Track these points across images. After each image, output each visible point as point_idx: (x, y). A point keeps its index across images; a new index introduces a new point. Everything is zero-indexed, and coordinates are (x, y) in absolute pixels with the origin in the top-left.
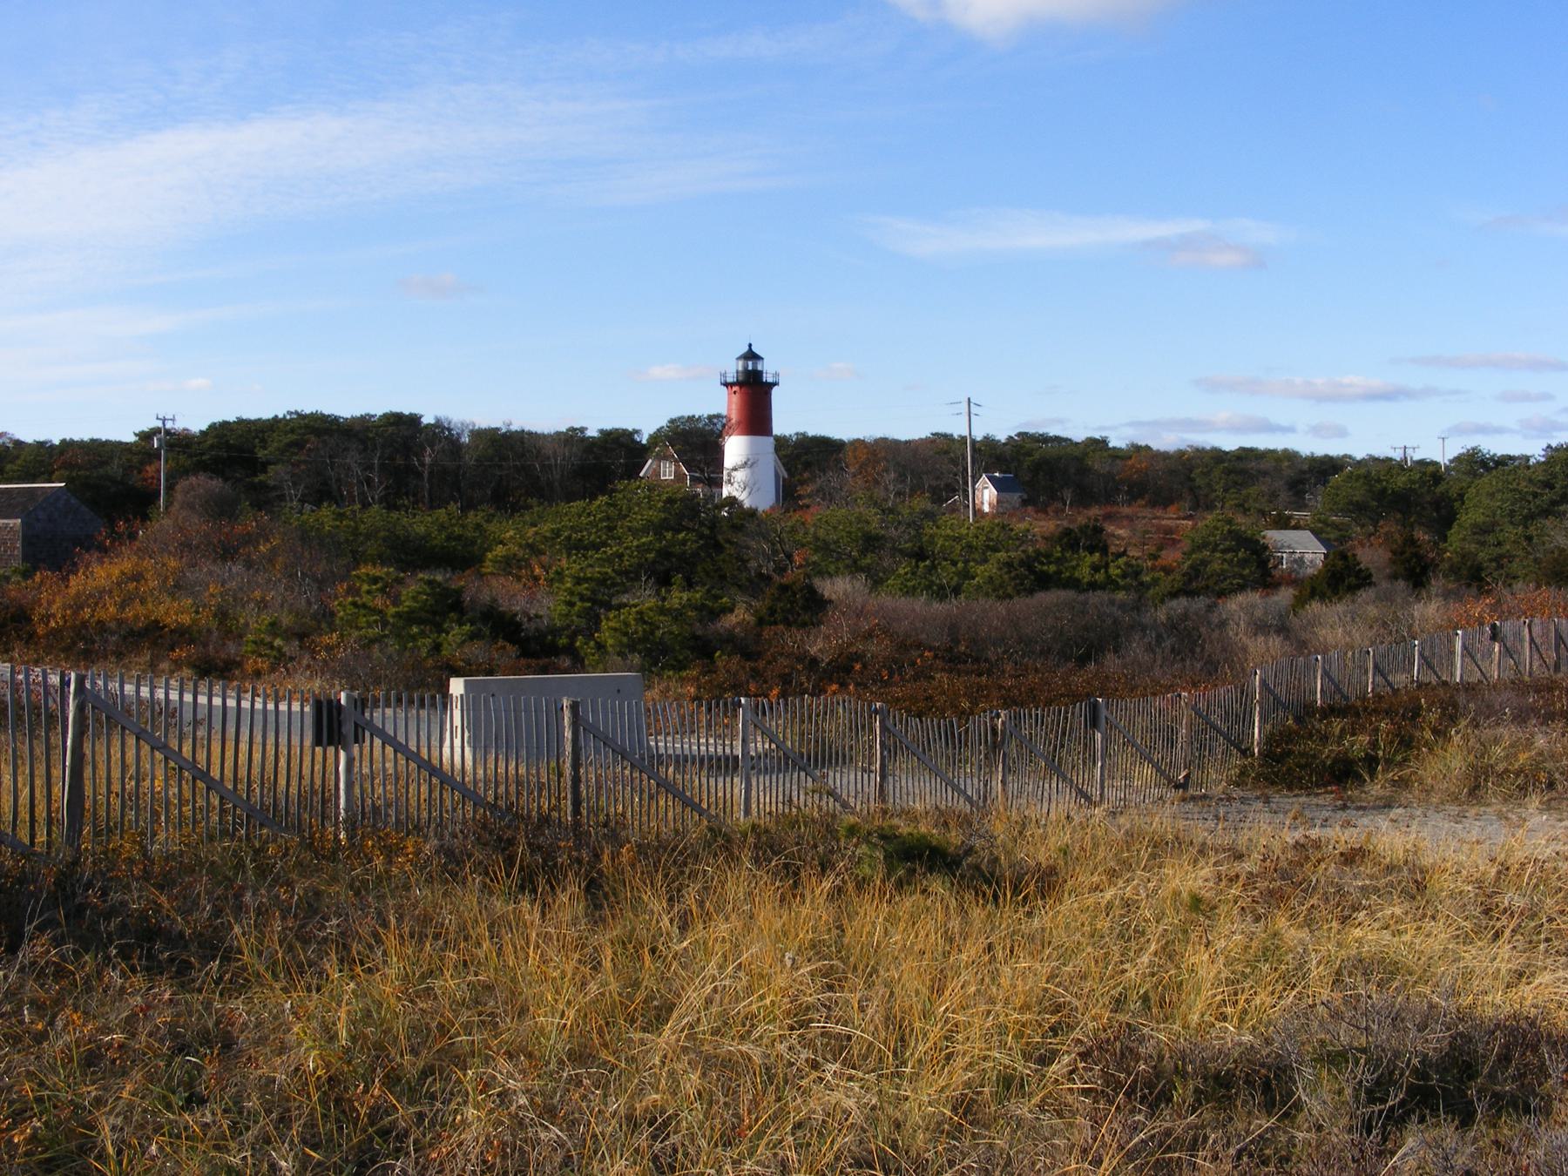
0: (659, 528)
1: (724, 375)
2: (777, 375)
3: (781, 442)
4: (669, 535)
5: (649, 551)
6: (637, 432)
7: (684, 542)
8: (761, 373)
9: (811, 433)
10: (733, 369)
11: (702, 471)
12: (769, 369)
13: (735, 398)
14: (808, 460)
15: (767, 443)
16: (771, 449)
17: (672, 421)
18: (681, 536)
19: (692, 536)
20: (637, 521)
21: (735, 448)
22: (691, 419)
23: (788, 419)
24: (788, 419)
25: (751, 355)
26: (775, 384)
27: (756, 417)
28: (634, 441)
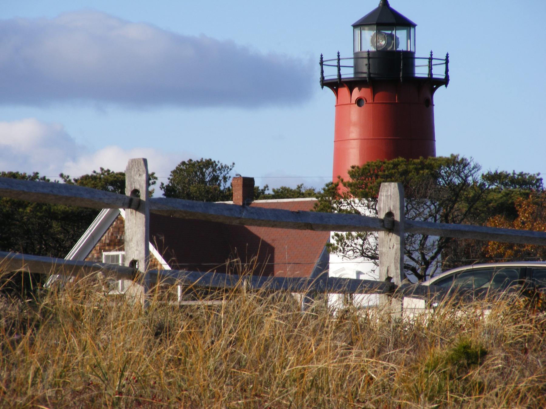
8: (408, 57)
10: (348, 46)
12: (425, 46)
13: (355, 113)
25: (387, 19)
26: (445, 81)
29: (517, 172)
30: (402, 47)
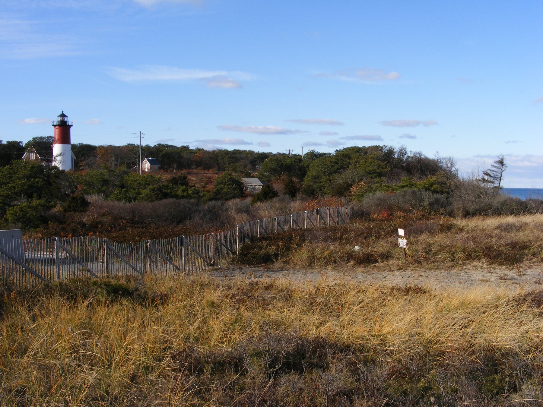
0: (29, 177)
1: (53, 122)
2: (72, 122)
3: (74, 147)
4: (32, 180)
5: (25, 185)
6: (21, 142)
7: (38, 182)
8: (66, 121)
9: (84, 143)
10: (57, 119)
11: (45, 157)
13: (57, 131)
14: (83, 153)
15: (69, 147)
16: (70, 149)
17: (34, 139)
18: (37, 180)
19: (41, 180)
20: (21, 175)
21: (57, 149)
22: (41, 138)
23: (77, 137)
24: (77, 137)
25: (63, 115)
26: (72, 126)
27: (65, 138)
28: (20, 146)
29: (457, 167)
30: (65, 120)
